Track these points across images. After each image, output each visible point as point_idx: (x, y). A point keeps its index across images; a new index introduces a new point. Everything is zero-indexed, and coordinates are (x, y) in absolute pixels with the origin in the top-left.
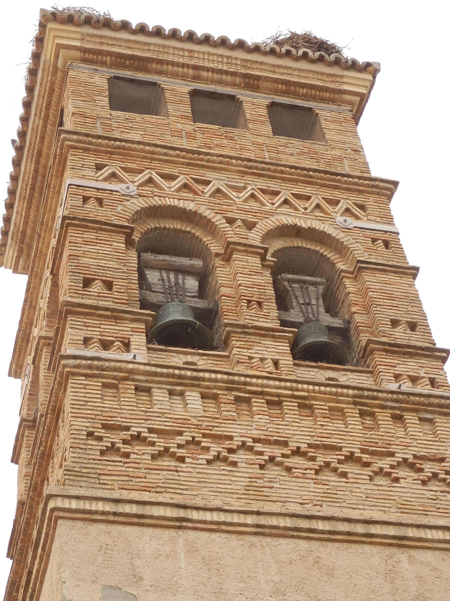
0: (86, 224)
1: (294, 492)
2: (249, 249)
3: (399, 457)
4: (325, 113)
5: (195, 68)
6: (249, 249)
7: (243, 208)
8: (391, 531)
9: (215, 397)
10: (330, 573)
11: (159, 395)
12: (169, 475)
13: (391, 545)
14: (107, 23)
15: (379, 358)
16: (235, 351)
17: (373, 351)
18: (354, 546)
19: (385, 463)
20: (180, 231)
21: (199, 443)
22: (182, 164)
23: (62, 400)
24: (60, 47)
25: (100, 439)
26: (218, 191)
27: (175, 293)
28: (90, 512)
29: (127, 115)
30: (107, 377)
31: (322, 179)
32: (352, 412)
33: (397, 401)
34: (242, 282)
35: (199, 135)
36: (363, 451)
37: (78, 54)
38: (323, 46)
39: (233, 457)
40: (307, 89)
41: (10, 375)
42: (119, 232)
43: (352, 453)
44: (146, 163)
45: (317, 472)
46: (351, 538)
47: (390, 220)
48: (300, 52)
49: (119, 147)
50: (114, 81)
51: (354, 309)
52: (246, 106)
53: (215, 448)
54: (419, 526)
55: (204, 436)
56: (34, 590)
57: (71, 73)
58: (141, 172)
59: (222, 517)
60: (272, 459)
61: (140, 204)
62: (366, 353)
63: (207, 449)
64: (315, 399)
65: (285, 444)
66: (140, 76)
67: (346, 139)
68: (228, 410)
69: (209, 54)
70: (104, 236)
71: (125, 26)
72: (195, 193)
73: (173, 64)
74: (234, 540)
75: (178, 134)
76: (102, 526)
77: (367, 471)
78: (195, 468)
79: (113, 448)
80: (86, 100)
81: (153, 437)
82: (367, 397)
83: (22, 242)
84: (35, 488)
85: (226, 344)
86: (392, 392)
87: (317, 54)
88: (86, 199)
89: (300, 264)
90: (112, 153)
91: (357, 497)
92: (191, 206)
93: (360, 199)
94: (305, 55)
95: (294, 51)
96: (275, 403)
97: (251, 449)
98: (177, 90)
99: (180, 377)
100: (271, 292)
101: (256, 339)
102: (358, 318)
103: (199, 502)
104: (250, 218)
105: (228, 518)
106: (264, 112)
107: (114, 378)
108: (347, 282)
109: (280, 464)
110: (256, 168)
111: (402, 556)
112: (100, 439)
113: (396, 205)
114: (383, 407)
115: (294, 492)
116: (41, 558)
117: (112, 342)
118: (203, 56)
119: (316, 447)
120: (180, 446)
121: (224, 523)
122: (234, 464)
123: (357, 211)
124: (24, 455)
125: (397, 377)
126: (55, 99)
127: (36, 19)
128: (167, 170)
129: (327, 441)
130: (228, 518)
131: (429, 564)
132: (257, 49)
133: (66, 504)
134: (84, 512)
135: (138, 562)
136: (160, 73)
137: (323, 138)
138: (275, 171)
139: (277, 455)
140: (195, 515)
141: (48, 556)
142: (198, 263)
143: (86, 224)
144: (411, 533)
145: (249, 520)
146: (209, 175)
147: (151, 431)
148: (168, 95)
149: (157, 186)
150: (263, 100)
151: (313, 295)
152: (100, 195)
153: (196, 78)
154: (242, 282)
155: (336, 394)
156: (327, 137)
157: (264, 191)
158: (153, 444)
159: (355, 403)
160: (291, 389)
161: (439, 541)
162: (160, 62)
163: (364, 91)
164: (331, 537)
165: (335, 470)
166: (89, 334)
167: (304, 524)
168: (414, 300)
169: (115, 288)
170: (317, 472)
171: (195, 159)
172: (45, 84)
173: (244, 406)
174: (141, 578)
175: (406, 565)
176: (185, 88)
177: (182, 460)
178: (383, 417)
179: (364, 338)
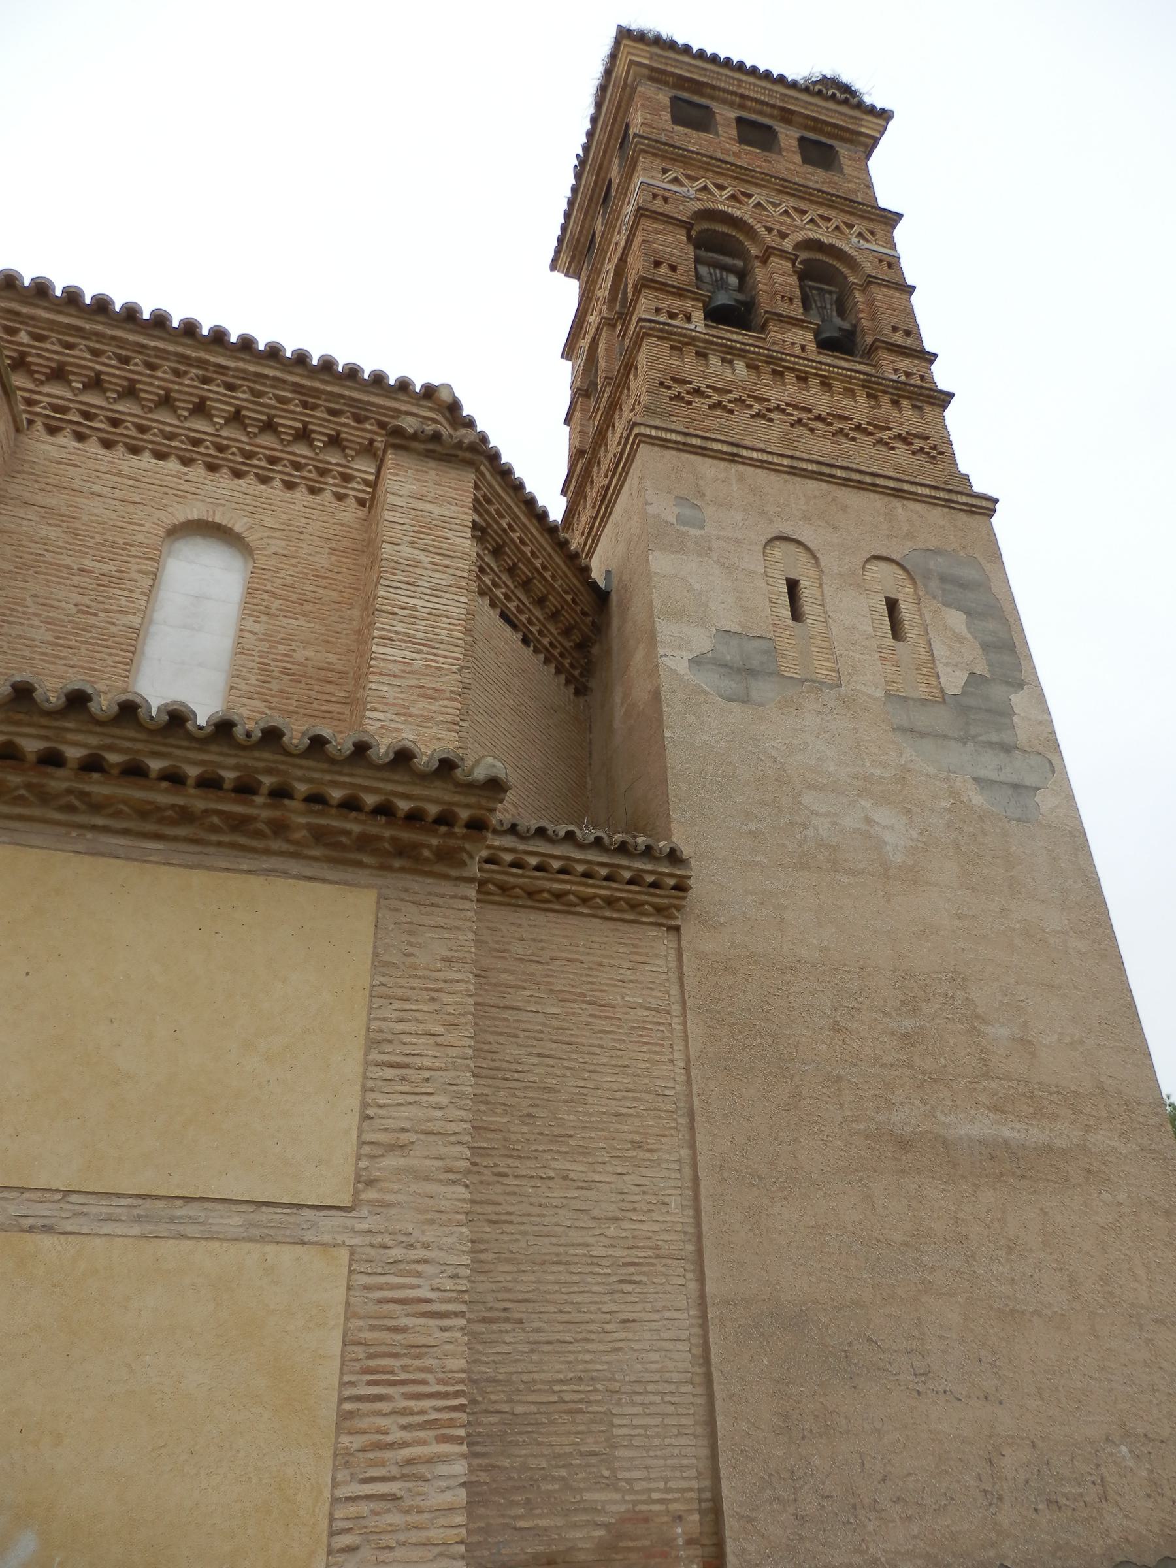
0: (656, 216)
1: (817, 446)
2: (783, 254)
3: (895, 432)
5: (742, 96)
6: (783, 254)
7: (779, 222)
8: (891, 484)
9: (756, 368)
10: (844, 509)
11: (714, 360)
12: (724, 422)
13: (889, 494)
14: (672, 45)
15: (882, 354)
16: (772, 334)
17: (877, 348)
18: (862, 492)
19: (885, 435)
20: (727, 234)
21: (744, 401)
22: (732, 177)
23: (635, 357)
24: (631, 62)
25: (669, 388)
26: (759, 204)
27: (721, 285)
28: (666, 440)
29: (687, 130)
30: (674, 340)
31: (842, 204)
33: (896, 388)
34: (776, 280)
35: (743, 156)
36: (869, 424)
37: (646, 72)
38: (846, 89)
39: (771, 415)
40: (831, 125)
41: (562, 357)
42: (682, 227)
43: (860, 424)
44: (702, 173)
45: (834, 435)
46: (860, 486)
47: (894, 247)
48: (830, 93)
49: (681, 155)
50: (675, 100)
51: (861, 315)
52: (781, 137)
53: (757, 407)
54: (912, 483)
55: (749, 396)
56: (609, 501)
57: (639, 89)
58: (698, 179)
59: (765, 457)
60: (800, 421)
61: (698, 206)
62: (872, 350)
63: (750, 407)
64: (834, 379)
65: (809, 411)
66: (696, 99)
67: (860, 175)
68: (766, 379)
69: (755, 85)
70: (671, 228)
71: (687, 49)
72: (740, 202)
74: (773, 476)
75: (726, 152)
76: (674, 453)
77: (870, 439)
78: (741, 418)
79: (678, 397)
80: (649, 114)
81: (710, 392)
82: (874, 383)
83: (575, 248)
84: (600, 433)
85: (763, 328)
86: (893, 381)
87: (844, 96)
88: (655, 196)
89: (822, 272)
90: (675, 160)
91: (863, 455)
92: (738, 213)
93: (871, 226)
94: (834, 95)
95: (825, 91)
96: (803, 378)
97: (783, 411)
98: (726, 115)
99: (731, 347)
100: (798, 293)
101: (789, 327)
102: (865, 323)
103: (749, 444)
104: (784, 229)
105: (770, 458)
106: (795, 143)
107: (680, 342)
108: (857, 294)
109: (805, 425)
110: (791, 188)
111: (898, 504)
112: (669, 388)
113: (900, 233)
114: (885, 392)
115: (817, 446)
116: (620, 475)
117: (677, 315)
118: (750, 88)
119: (833, 415)
120: (730, 402)
121: (766, 462)
122: (771, 420)
123: (869, 236)
124: (577, 415)
125: (896, 371)
126: (620, 114)
127: (613, 33)
128: (719, 181)
129: (842, 413)
130: (770, 458)
131: (917, 512)
132: (794, 85)
133: (648, 431)
134: (661, 439)
135: (702, 483)
136: (712, 98)
137: (841, 171)
138: (805, 193)
139: (805, 419)
140: (745, 453)
141: (627, 474)
142: (739, 263)
143: (656, 216)
144: (906, 487)
145: (786, 462)
146: (753, 190)
147: (708, 387)
148: (718, 117)
149: (710, 193)
150: (795, 134)
151: (828, 302)
152: (666, 194)
153: (742, 107)
154: (776, 280)
155: (850, 377)
156: (846, 171)
157: (795, 209)
158: (709, 397)
159: (864, 386)
160: (815, 368)
161: (927, 496)
162: (714, 87)
163: (878, 135)
164: (845, 483)
165: (847, 435)
166: (660, 305)
167: (827, 470)
168: (910, 313)
169: (678, 271)
170: (834, 435)
171: (743, 174)
172: (613, 96)
173: (778, 378)
174: (704, 495)
175: (900, 511)
176: (733, 114)
177: (731, 412)
178: (885, 401)
179: (869, 339)
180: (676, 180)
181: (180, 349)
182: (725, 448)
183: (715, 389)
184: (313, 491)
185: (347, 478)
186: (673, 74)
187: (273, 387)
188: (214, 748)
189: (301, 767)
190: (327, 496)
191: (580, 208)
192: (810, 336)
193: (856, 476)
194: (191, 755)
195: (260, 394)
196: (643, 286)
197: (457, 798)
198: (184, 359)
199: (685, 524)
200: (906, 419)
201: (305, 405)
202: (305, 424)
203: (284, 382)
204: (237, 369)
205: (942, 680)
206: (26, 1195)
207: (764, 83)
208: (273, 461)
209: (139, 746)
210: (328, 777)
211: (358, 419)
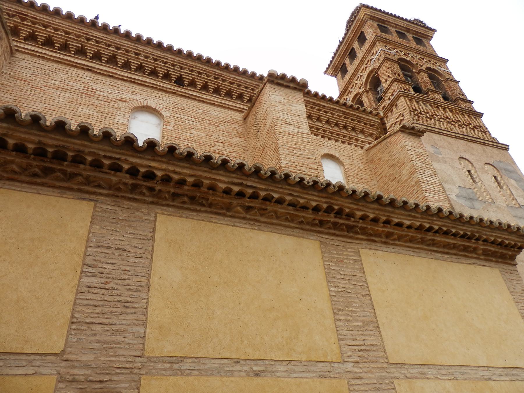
4: (424, 40)
5: (396, 24)
11: (421, 103)
24: (365, 14)
26: (412, 57)
32: (460, 113)
37: (369, 17)
46: (474, 142)
68: (435, 109)
73: (391, 22)
78: (434, 121)
81: (423, 113)
118: (398, 21)
128: (400, 49)
132: (409, 21)
136: (387, 25)
140: (443, 132)
143: (390, 60)
144: (486, 142)
162: (388, 22)
177: (431, 119)
180: (389, 49)
181: (313, 101)
182: (438, 130)
183: (425, 112)
184: (349, 144)
185: (357, 140)
186: (377, 18)
187: (337, 112)
188: (466, 225)
189: (485, 231)
190: (353, 146)
191: (339, 56)
192: (441, 96)
193: (473, 139)
194: (461, 227)
195: (334, 114)
196: (395, 81)
197: (518, 240)
198: (314, 104)
199: (437, 154)
200: (473, 121)
201: (345, 117)
202: (346, 123)
203: (340, 110)
204: (328, 107)
205: (518, 201)
206: (480, 368)
207: (401, 21)
208: (338, 135)
209: (450, 225)
210: (491, 234)
211: (359, 122)
